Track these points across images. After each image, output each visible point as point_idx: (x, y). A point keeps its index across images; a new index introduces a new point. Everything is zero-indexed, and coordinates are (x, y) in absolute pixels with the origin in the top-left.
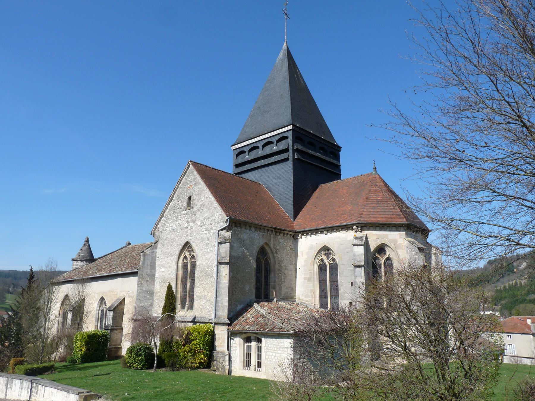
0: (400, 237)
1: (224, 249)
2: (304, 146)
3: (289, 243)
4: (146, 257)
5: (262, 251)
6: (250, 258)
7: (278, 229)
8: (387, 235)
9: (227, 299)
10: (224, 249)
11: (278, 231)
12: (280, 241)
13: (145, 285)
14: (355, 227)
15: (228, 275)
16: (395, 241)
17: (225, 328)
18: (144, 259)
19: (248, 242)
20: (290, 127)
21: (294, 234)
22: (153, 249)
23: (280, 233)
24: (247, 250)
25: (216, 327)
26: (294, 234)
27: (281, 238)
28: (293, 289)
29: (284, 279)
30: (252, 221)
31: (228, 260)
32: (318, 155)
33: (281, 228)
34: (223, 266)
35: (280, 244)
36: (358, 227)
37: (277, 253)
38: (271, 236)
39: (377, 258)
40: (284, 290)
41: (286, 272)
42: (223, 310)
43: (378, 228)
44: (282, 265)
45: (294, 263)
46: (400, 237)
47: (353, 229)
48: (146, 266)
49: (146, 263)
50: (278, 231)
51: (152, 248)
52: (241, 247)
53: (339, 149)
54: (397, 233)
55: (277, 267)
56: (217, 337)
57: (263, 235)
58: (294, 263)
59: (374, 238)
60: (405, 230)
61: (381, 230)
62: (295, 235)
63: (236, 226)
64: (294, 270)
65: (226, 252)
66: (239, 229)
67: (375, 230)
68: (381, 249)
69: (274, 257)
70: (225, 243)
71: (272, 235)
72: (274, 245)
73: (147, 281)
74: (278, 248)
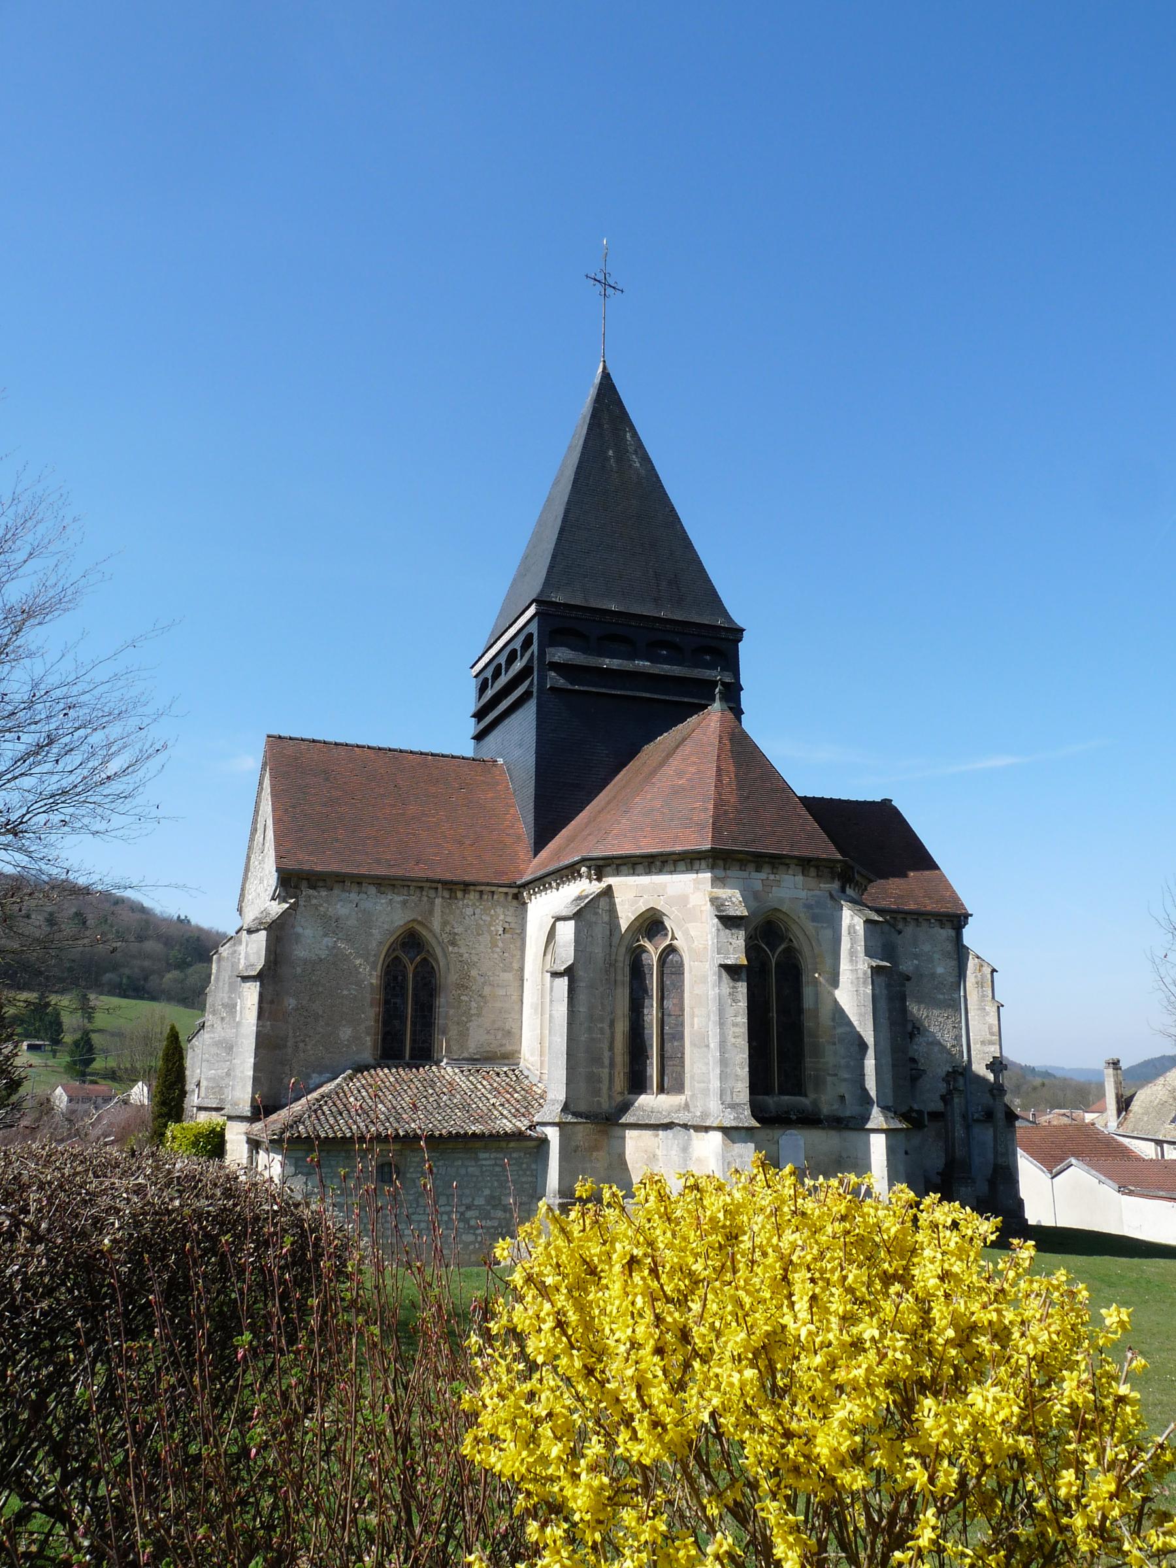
0: (697, 889)
1: (254, 945)
2: (585, 651)
3: (502, 915)
4: (223, 963)
5: (411, 941)
6: (358, 962)
7: (457, 883)
8: (664, 886)
9: (252, 1060)
10: (254, 945)
11: (456, 888)
12: (469, 911)
13: (219, 1029)
14: (583, 869)
15: (256, 1006)
16: (683, 900)
17: (243, 1127)
18: (219, 968)
19: (352, 922)
20: (532, 610)
21: (515, 890)
22: (234, 945)
23: (465, 891)
24: (348, 940)
25: (229, 1124)
26: (515, 890)
27: (469, 905)
28: (512, 1034)
29: (480, 1008)
30: (363, 871)
31: (952, 933)
32: (643, 665)
33: (467, 878)
34: (248, 984)
35: (467, 921)
36: (589, 868)
37: (453, 943)
38: (432, 903)
39: (643, 949)
40: (477, 1038)
41: (487, 991)
42: (244, 1086)
43: (681, 866)
44: (474, 973)
45: (516, 966)
46: (697, 889)
47: (580, 876)
48: (221, 984)
49: (221, 978)
50: (456, 888)
51: (231, 942)
52: (326, 935)
53: (737, 633)
54: (690, 877)
55: (453, 978)
56: (228, 1146)
57: (404, 903)
58: (516, 966)
59: (631, 895)
60: (712, 868)
61: (648, 872)
62: (518, 894)
63: (314, 887)
64: (517, 984)
65: (258, 953)
66: (324, 893)
67: (634, 874)
68: (652, 924)
69: (445, 955)
70: (258, 930)
71: (438, 901)
72: (445, 923)
73: (223, 1019)
74: (459, 930)
